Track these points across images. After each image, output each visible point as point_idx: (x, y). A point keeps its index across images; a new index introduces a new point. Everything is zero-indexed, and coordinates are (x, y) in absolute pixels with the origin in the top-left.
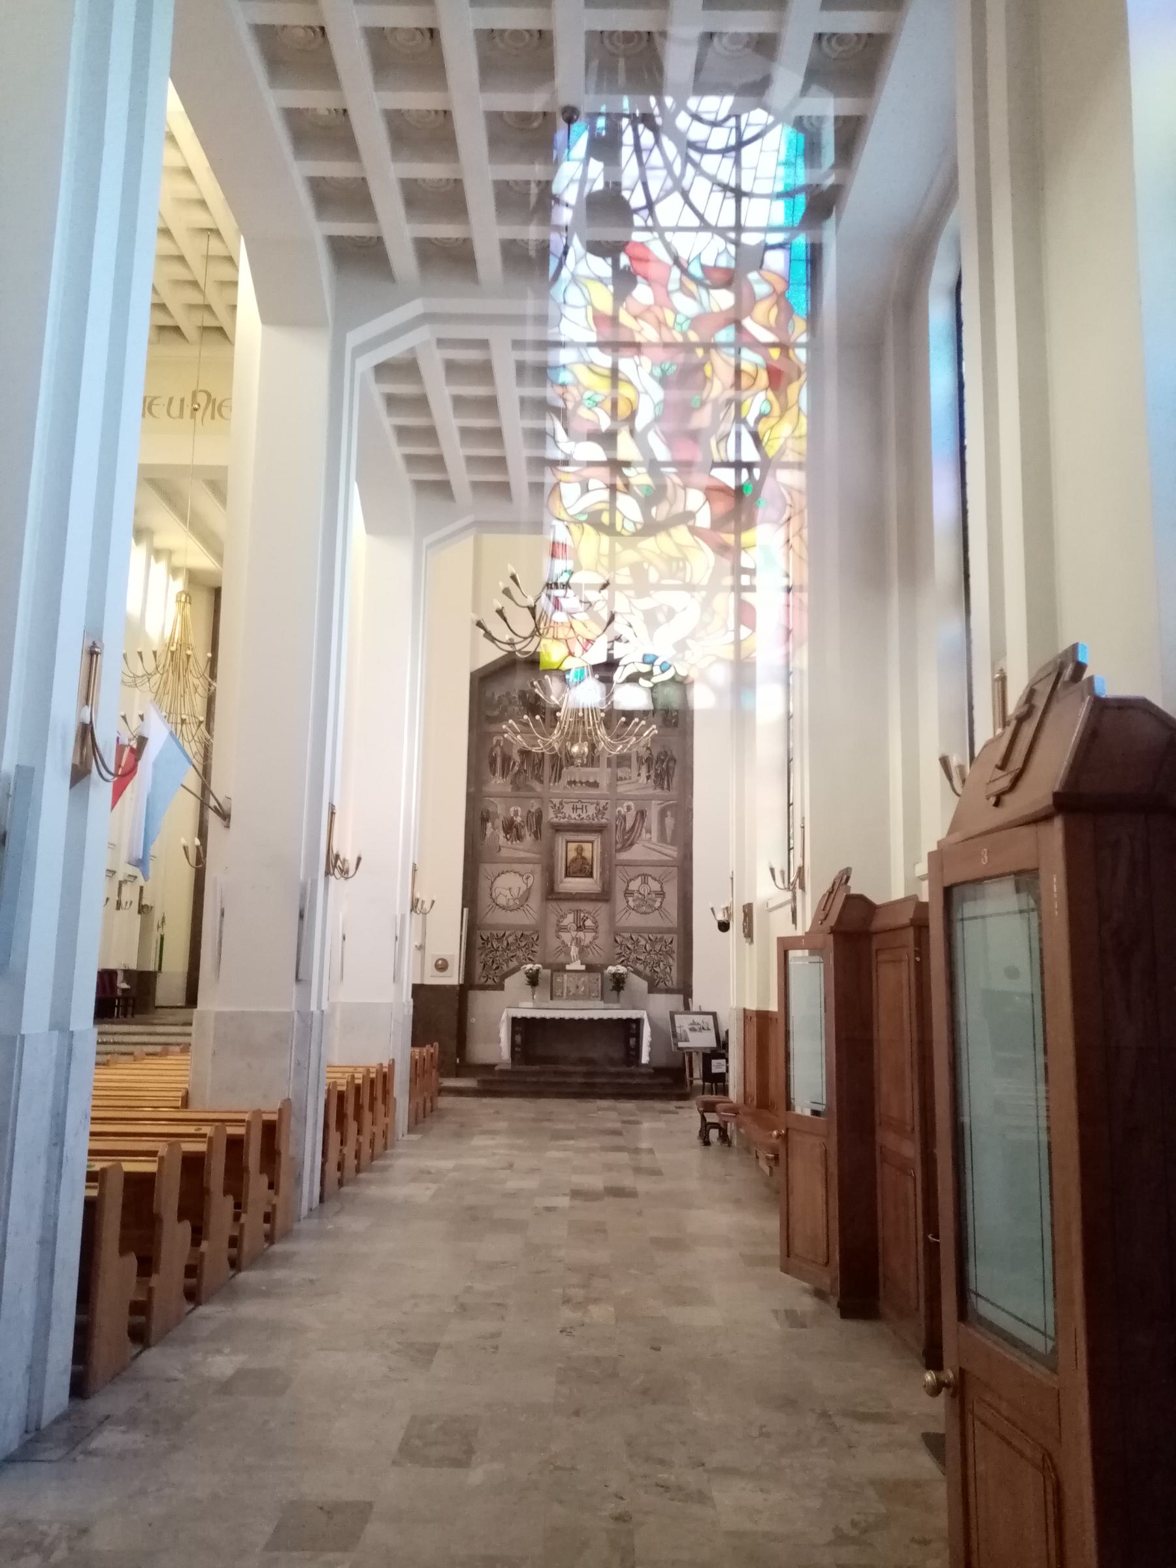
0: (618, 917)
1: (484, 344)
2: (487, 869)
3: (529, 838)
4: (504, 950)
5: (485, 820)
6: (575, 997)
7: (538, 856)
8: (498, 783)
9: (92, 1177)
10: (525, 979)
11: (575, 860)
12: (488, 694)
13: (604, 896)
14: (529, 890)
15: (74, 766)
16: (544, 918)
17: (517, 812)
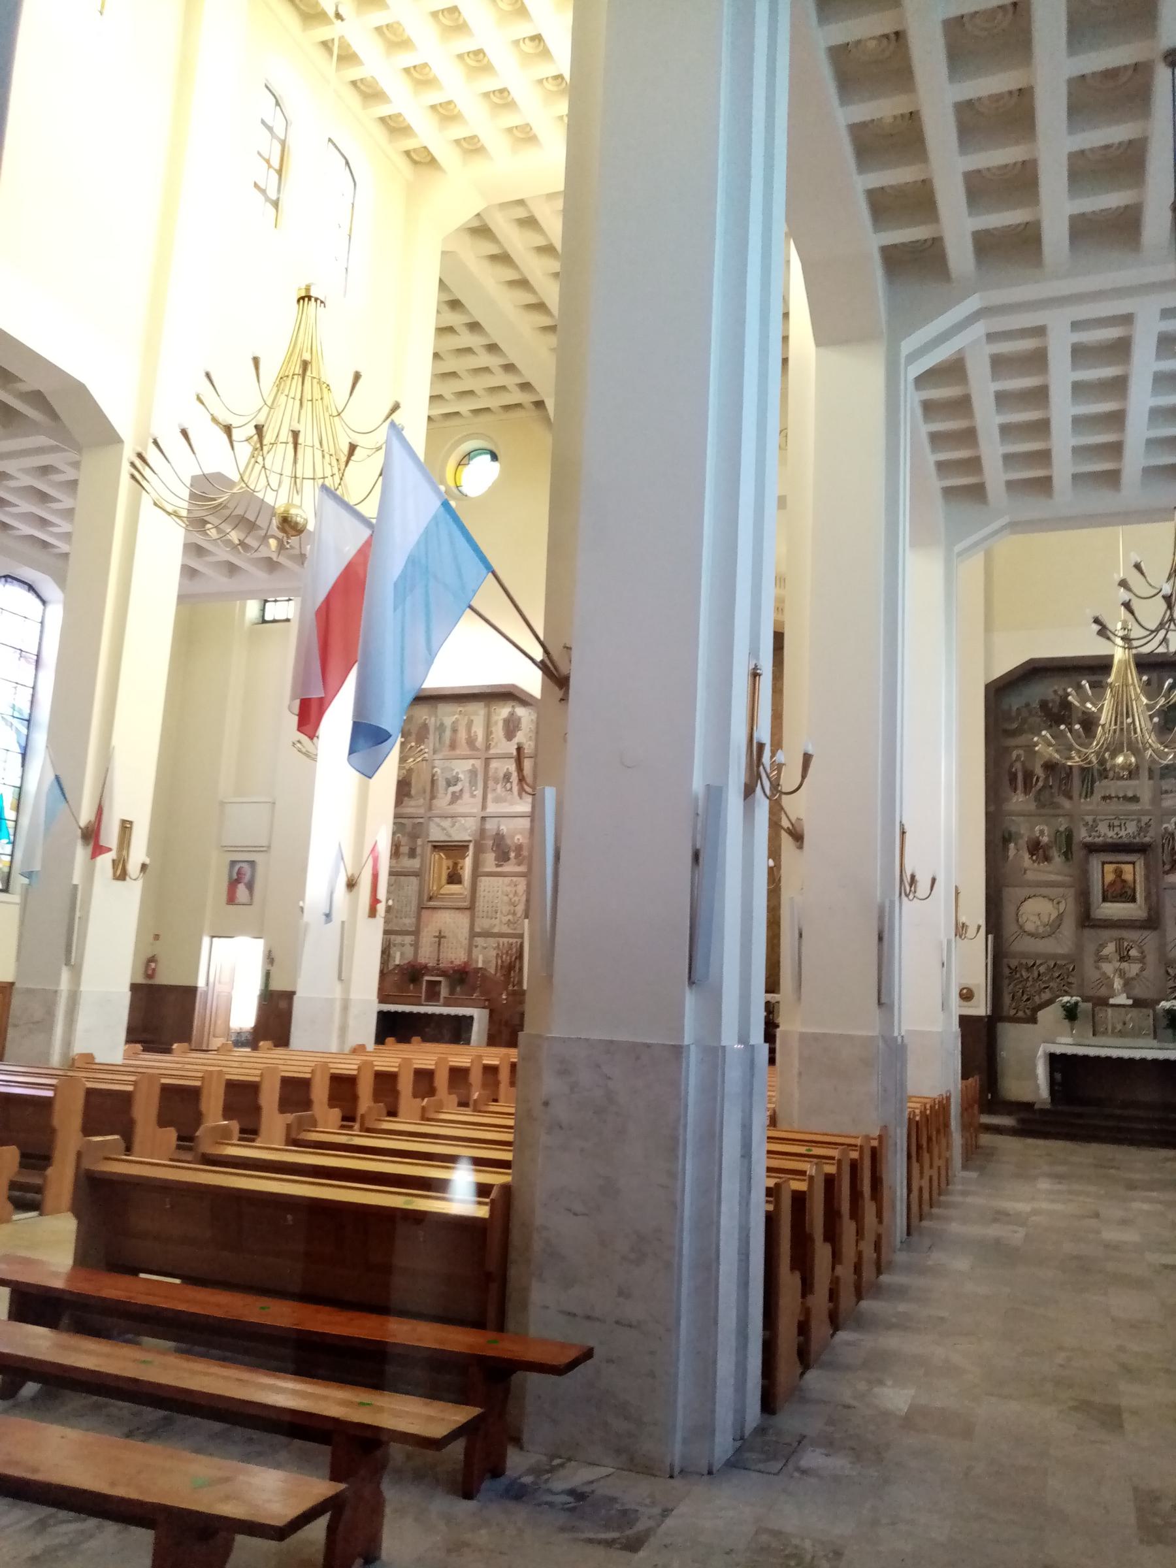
0: (1169, 948)
1: (1040, 331)
2: (1012, 894)
3: (1058, 859)
4: (1035, 980)
5: (1007, 838)
6: (1122, 1034)
7: (1067, 879)
8: (1019, 801)
9: (769, 1192)
10: (1061, 1013)
11: (1112, 884)
12: (1005, 707)
13: (1152, 922)
14: (1060, 916)
15: (746, 785)
16: (1079, 947)
17: (1044, 832)
